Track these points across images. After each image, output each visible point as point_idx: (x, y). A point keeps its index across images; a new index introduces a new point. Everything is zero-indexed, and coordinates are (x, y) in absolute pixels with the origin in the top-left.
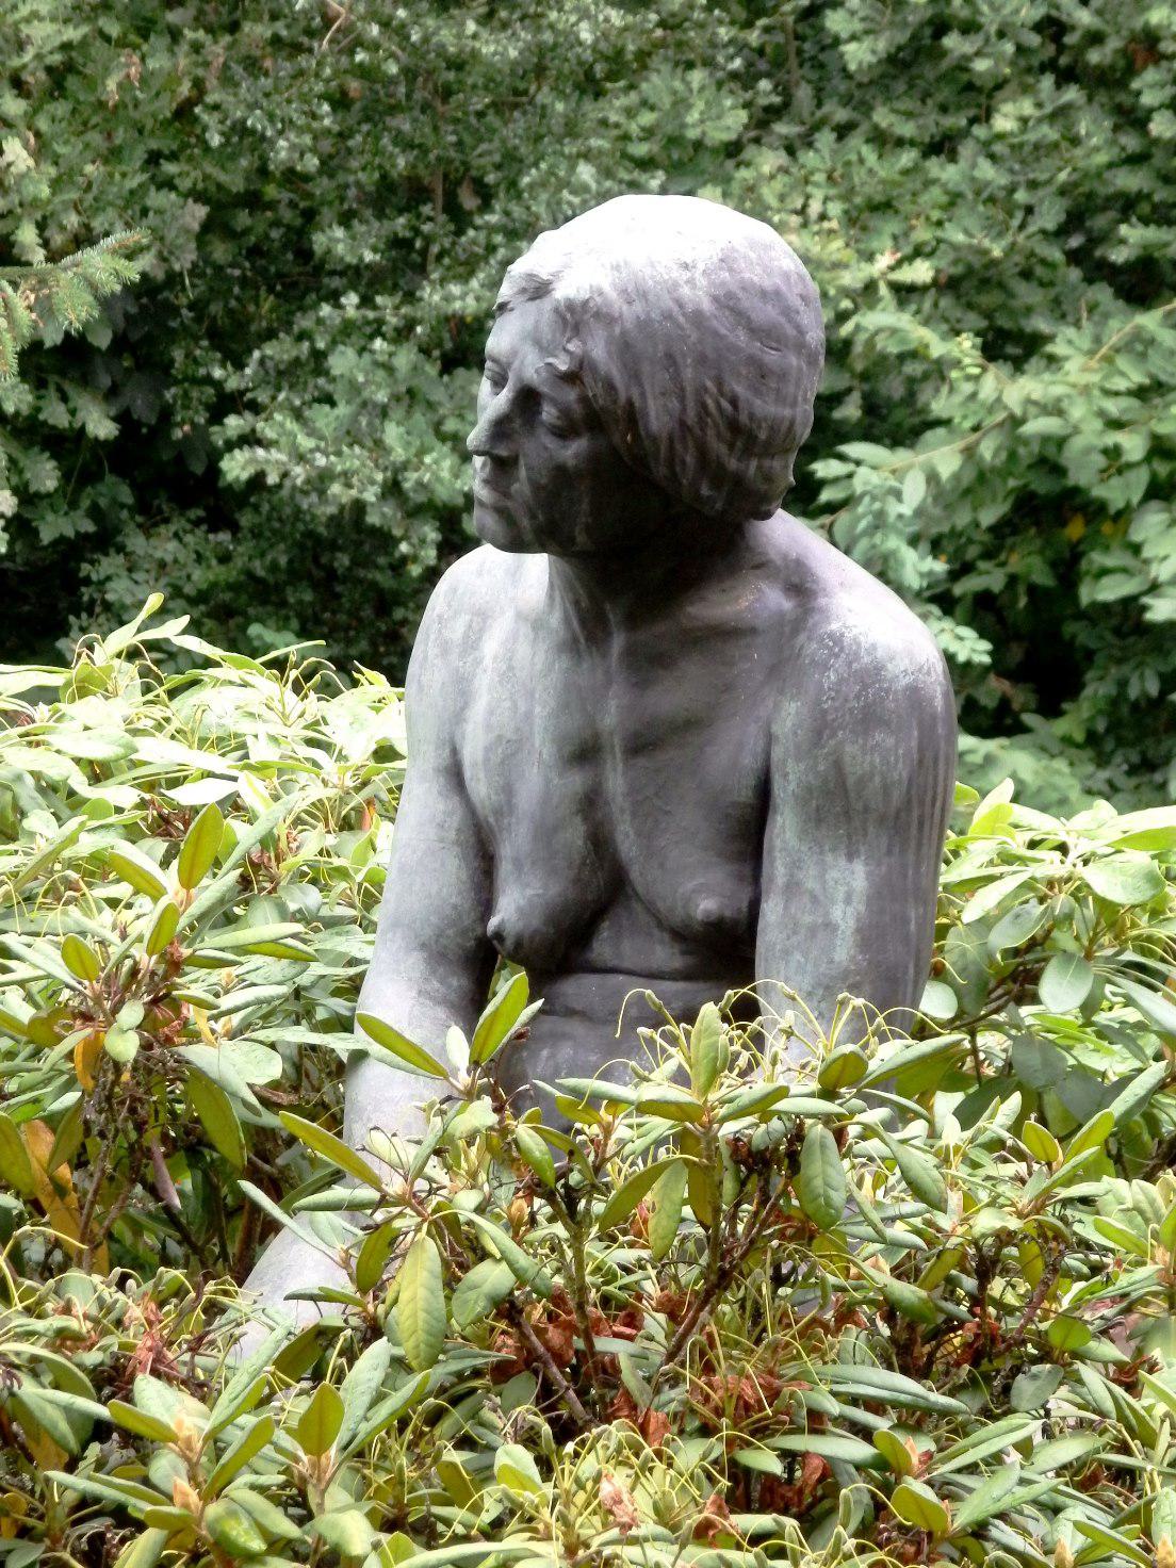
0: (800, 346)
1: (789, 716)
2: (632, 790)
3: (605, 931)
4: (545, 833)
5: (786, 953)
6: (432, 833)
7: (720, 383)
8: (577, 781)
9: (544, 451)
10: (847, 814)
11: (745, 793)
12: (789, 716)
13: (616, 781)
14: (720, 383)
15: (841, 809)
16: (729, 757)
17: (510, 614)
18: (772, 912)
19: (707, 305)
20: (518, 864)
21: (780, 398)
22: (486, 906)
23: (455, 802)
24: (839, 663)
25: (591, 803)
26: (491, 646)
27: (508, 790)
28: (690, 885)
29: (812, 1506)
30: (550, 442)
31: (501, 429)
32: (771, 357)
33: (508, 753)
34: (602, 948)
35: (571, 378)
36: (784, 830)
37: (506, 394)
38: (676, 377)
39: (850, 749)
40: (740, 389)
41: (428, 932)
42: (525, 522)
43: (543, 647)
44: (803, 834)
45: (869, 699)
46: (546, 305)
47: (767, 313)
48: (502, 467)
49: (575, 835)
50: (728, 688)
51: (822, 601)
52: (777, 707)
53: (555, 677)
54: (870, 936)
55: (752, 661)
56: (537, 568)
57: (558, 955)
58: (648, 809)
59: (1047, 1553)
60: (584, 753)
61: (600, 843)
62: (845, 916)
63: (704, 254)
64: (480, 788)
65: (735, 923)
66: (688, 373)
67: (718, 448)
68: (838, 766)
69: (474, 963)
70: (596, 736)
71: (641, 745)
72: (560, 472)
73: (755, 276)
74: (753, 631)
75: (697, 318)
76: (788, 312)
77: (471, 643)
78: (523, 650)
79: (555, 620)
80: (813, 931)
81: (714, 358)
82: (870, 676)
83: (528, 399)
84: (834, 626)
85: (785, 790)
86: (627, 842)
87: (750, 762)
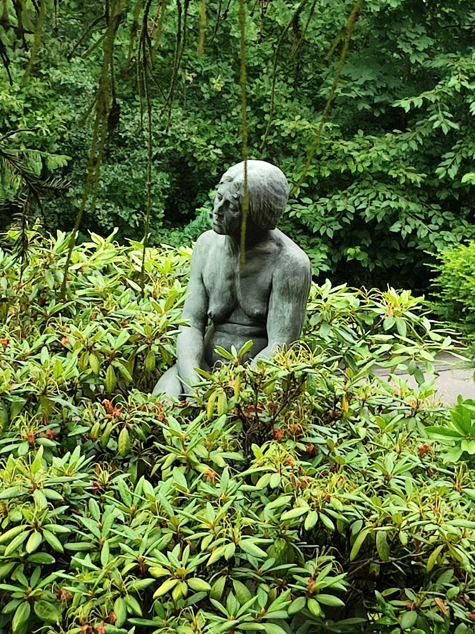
0: (285, 194)
1: (277, 272)
2: (241, 285)
3: (233, 315)
4: (222, 294)
5: (274, 322)
6: (196, 292)
7: (268, 202)
8: (229, 283)
9: (230, 213)
10: (289, 293)
11: (266, 287)
12: (277, 272)
13: (238, 283)
14: (268, 202)
15: (287, 292)
16: (263, 279)
17: (215, 246)
18: (271, 313)
19: (266, 185)
20: (215, 299)
21: (280, 205)
22: (207, 308)
23: (201, 285)
24: (289, 261)
25: (232, 288)
26: (211, 252)
27: (214, 284)
28: (253, 307)
29: (425, 164)
30: (231, 212)
31: (221, 209)
32: (279, 196)
33: (214, 277)
34: (232, 319)
35: (237, 199)
36: (275, 296)
37: (222, 201)
38: (260, 200)
39: (290, 280)
40: (272, 203)
41: (195, 313)
42: (224, 229)
43: (223, 254)
44: (279, 297)
45: (295, 270)
46: (232, 183)
47: (278, 187)
48: (220, 217)
49: (228, 294)
50: (264, 265)
51: (284, 248)
52: (275, 270)
53: (226, 261)
54: (293, 320)
55: (271, 258)
56: (222, 238)
57: (222, 319)
58: (245, 290)
59: (305, 587)
60: (231, 277)
61: (233, 296)
62: (288, 315)
63: (266, 175)
64: (207, 283)
65: (262, 315)
66: (262, 199)
67: (266, 215)
68: (288, 283)
69: (203, 319)
70: (234, 273)
71: (244, 276)
72: (233, 218)
73: (277, 179)
74: (270, 253)
75: (264, 187)
76: (283, 187)
77: (206, 251)
78: (218, 254)
79: (226, 248)
80: (280, 318)
81: (267, 196)
82: (296, 264)
83: (227, 203)
84: (288, 253)
85: (276, 287)
86: (239, 296)
87: (268, 281)
